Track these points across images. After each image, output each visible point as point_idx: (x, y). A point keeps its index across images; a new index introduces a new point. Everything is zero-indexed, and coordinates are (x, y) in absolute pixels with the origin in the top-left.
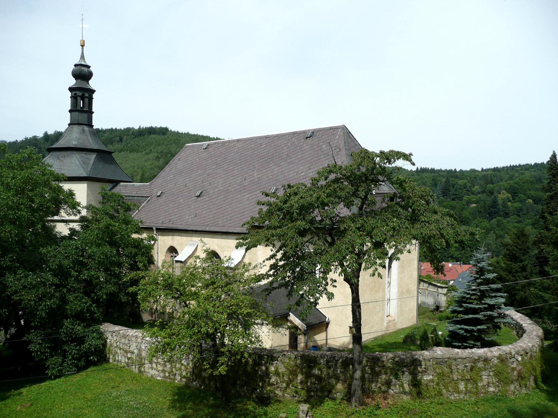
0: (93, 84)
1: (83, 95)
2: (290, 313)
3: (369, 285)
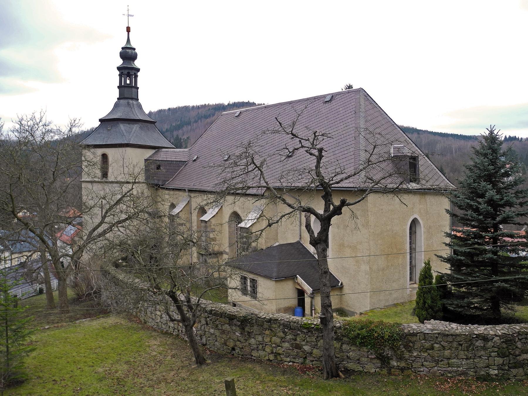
0: (137, 63)
1: (129, 73)
2: (298, 276)
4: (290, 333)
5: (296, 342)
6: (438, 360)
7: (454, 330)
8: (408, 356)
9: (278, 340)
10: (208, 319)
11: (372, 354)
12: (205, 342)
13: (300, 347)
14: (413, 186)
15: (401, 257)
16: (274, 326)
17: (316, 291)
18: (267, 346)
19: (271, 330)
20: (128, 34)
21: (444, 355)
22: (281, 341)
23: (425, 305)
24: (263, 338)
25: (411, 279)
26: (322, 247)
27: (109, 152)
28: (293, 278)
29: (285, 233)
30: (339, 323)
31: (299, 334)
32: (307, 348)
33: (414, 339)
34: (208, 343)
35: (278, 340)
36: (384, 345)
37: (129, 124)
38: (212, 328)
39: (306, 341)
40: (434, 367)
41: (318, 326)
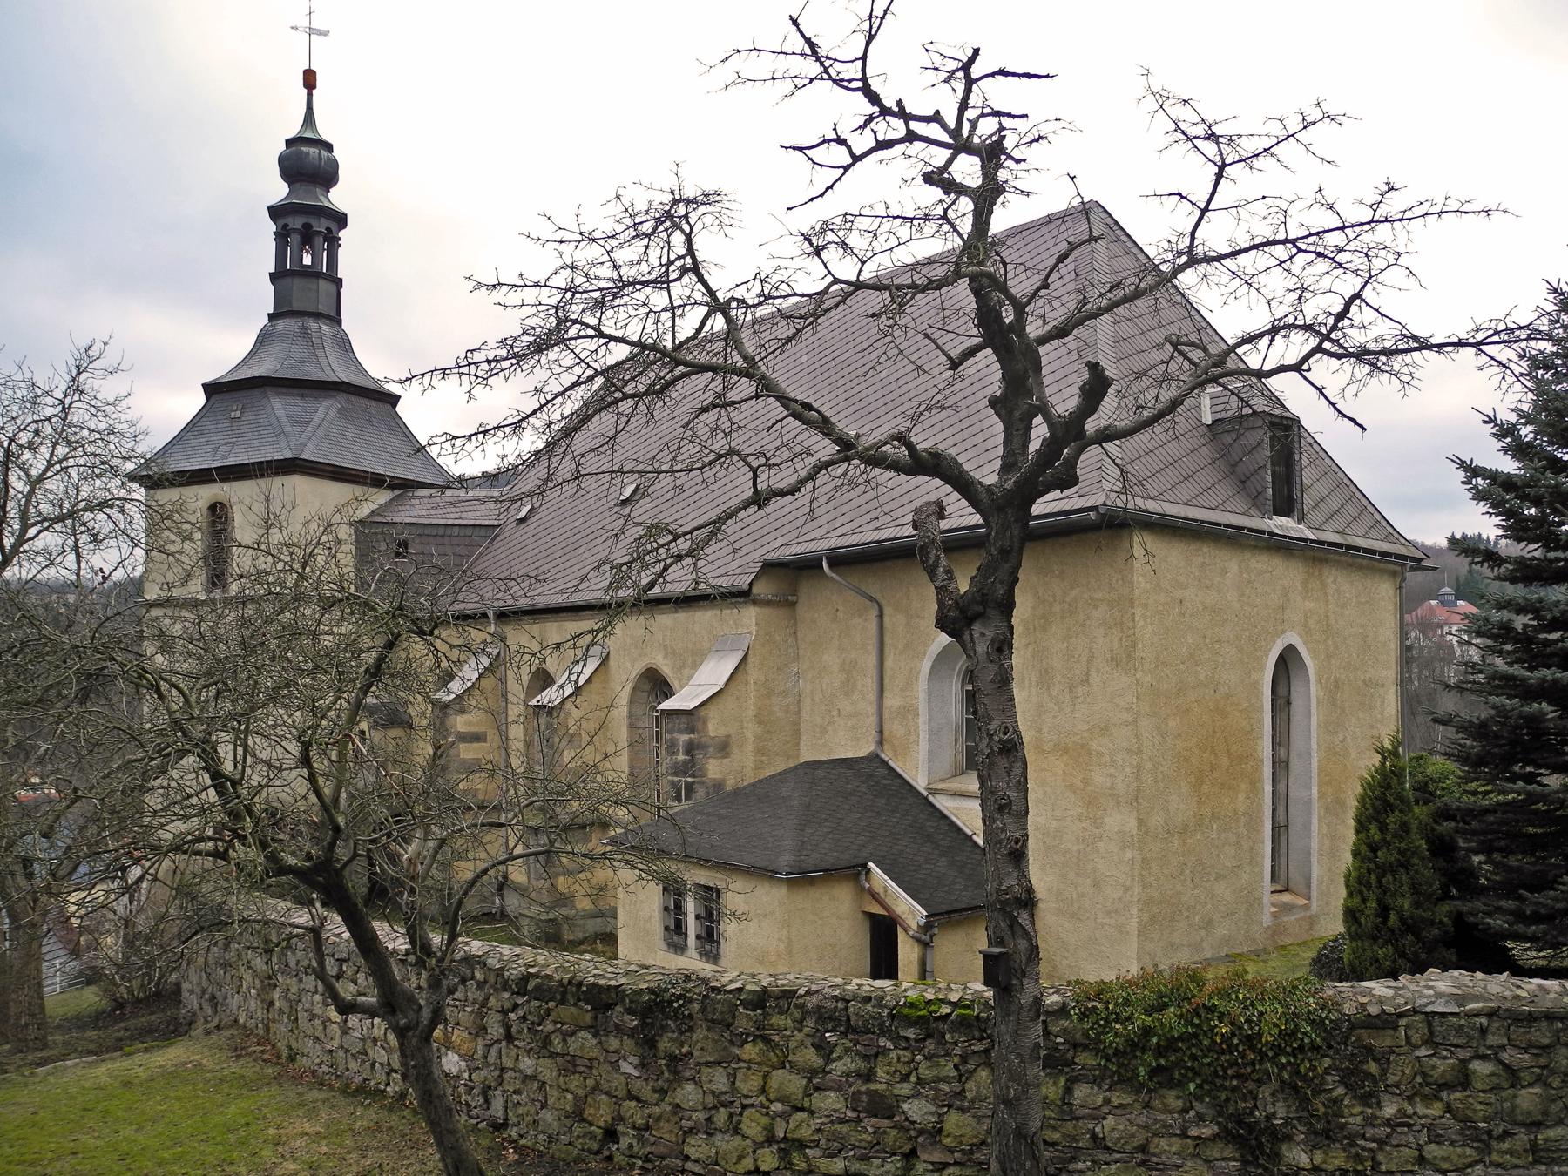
0: (338, 197)
1: (307, 226)
2: (871, 865)
3: (1186, 760)
4: (847, 1050)
5: (873, 1087)
6: (1489, 1132)
7: (1552, 995)
8: (1359, 1119)
9: (794, 1084)
10: (512, 1016)
11: (1200, 1118)
12: (500, 1114)
13: (891, 1107)
14: (1281, 524)
15: (1243, 786)
16: (778, 1020)
17: (942, 918)
18: (746, 1113)
19: (767, 1040)
20: (310, 96)
21: (1514, 1107)
22: (806, 1088)
23: (1386, 919)
24: (732, 1078)
25: (1274, 879)
26: (990, 634)
27: (238, 493)
28: (854, 872)
29: (824, 731)
30: (1057, 991)
31: (885, 1051)
32: (917, 1110)
33: (1382, 1041)
34: (513, 1119)
35: (794, 1084)
36: (1255, 1077)
37: (303, 396)
38: (528, 1052)
39: (913, 1079)
40: (1471, 1165)
41: (966, 1007)
